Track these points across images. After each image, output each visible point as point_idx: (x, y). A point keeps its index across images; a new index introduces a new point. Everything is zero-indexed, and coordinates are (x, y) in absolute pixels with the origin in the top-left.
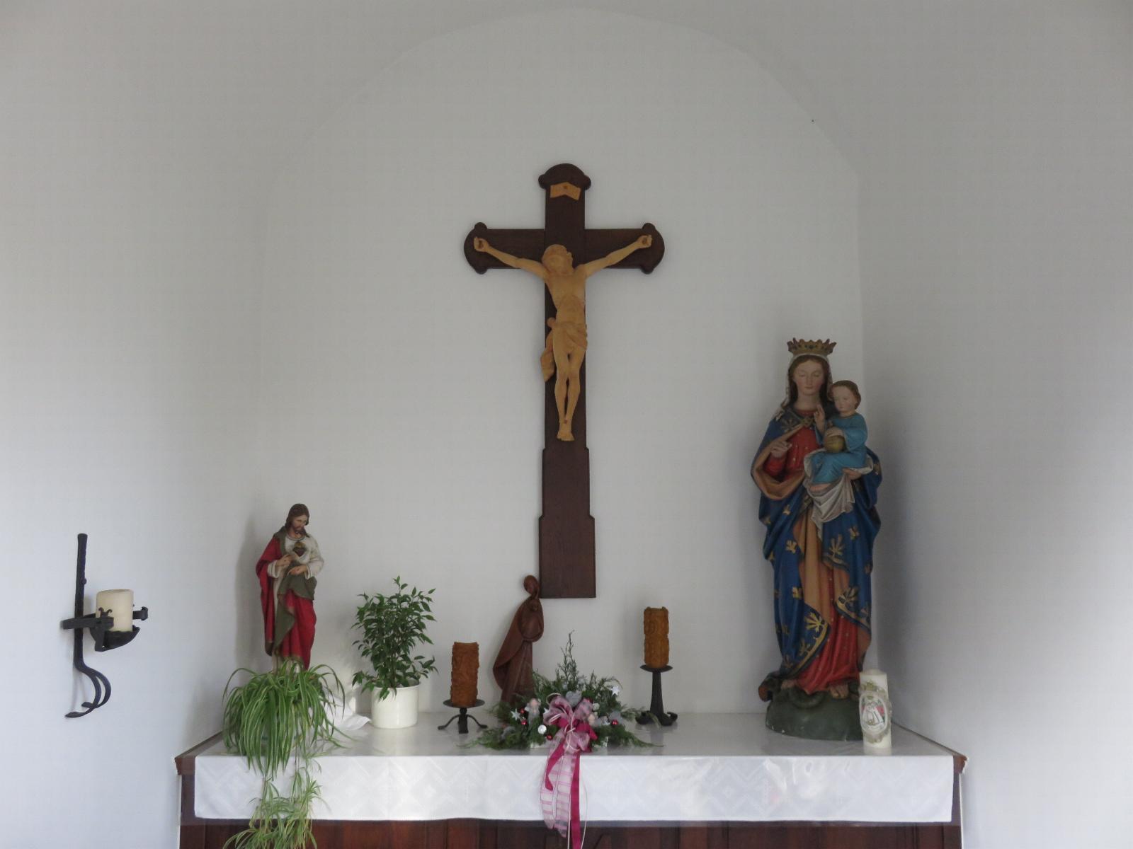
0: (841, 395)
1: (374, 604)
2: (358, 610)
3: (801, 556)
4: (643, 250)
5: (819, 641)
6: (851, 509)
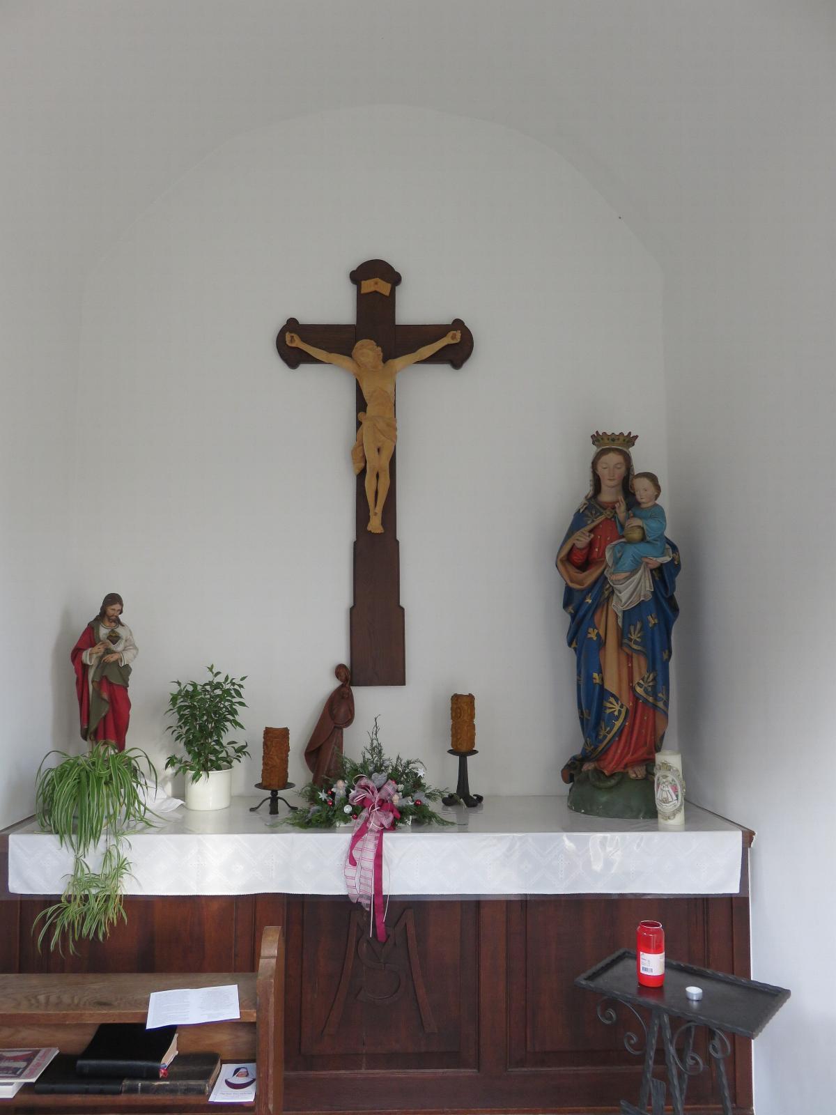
0: (641, 487)
1: (187, 691)
3: (602, 643)
4: (453, 346)
5: (618, 724)
6: (650, 596)
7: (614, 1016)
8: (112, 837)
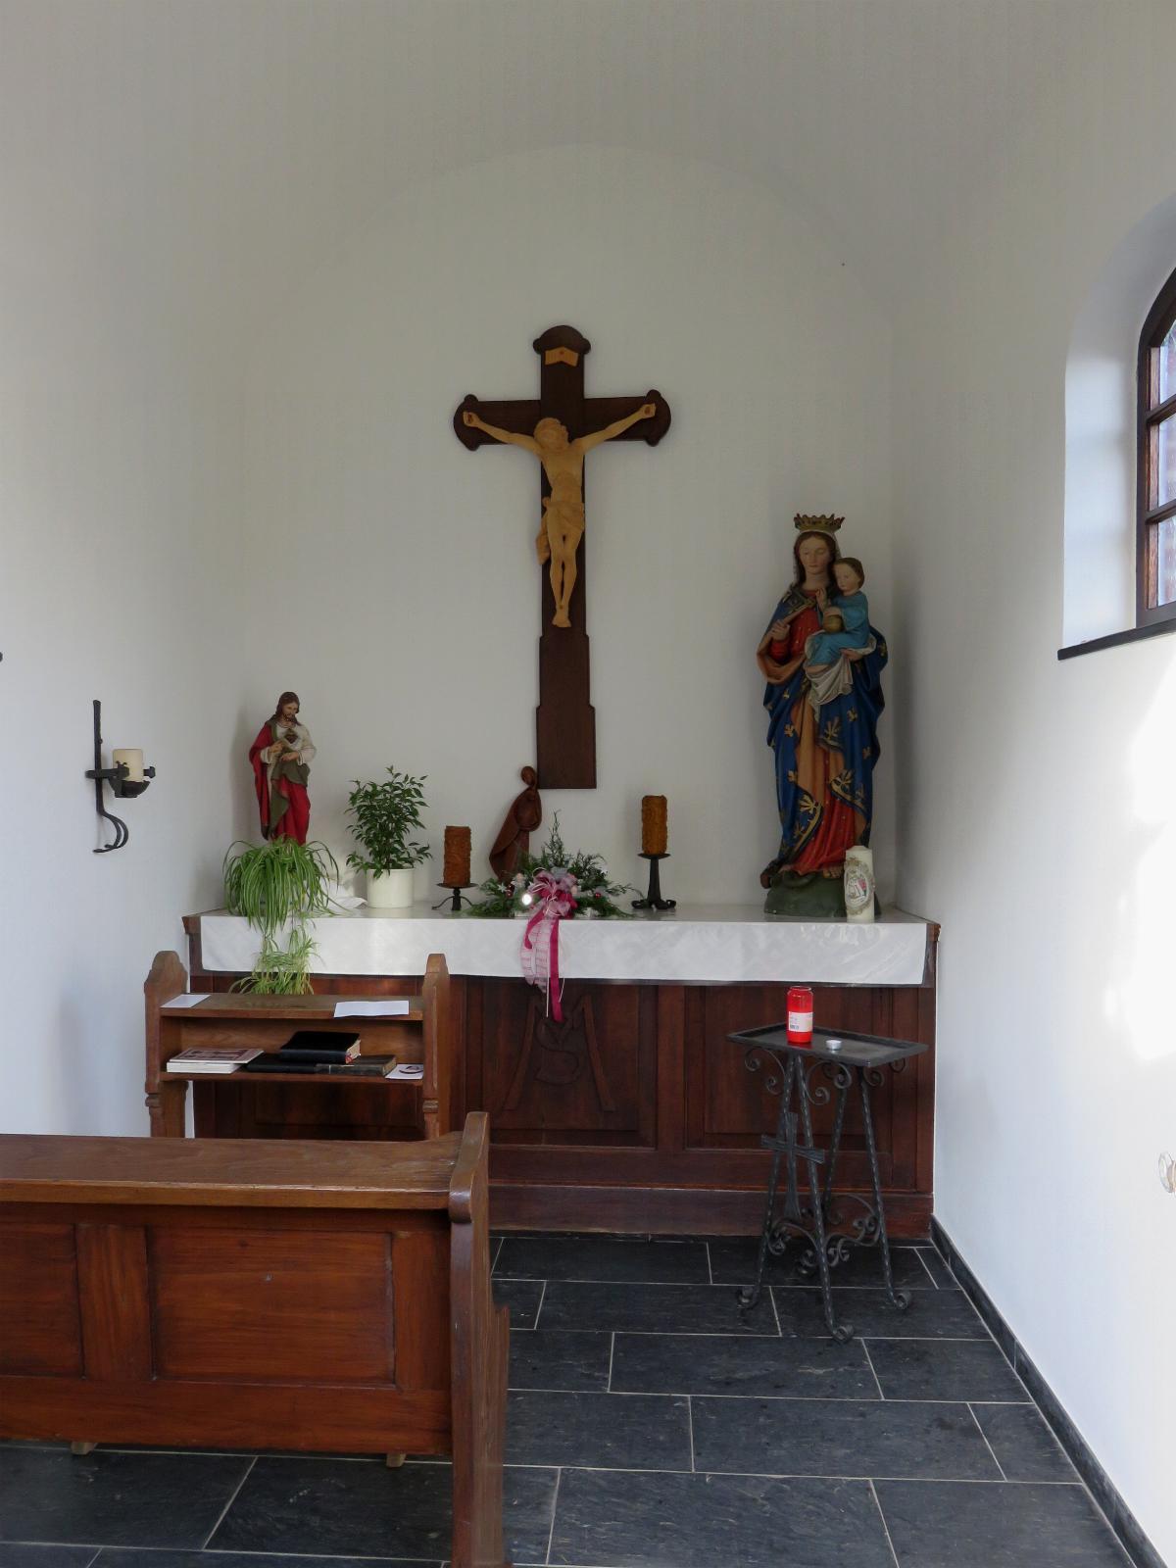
0: (843, 572)
2: (350, 796)
3: (797, 740)
4: (648, 419)
5: (813, 823)
6: (849, 691)
7: (758, 1063)
8: (297, 919)
